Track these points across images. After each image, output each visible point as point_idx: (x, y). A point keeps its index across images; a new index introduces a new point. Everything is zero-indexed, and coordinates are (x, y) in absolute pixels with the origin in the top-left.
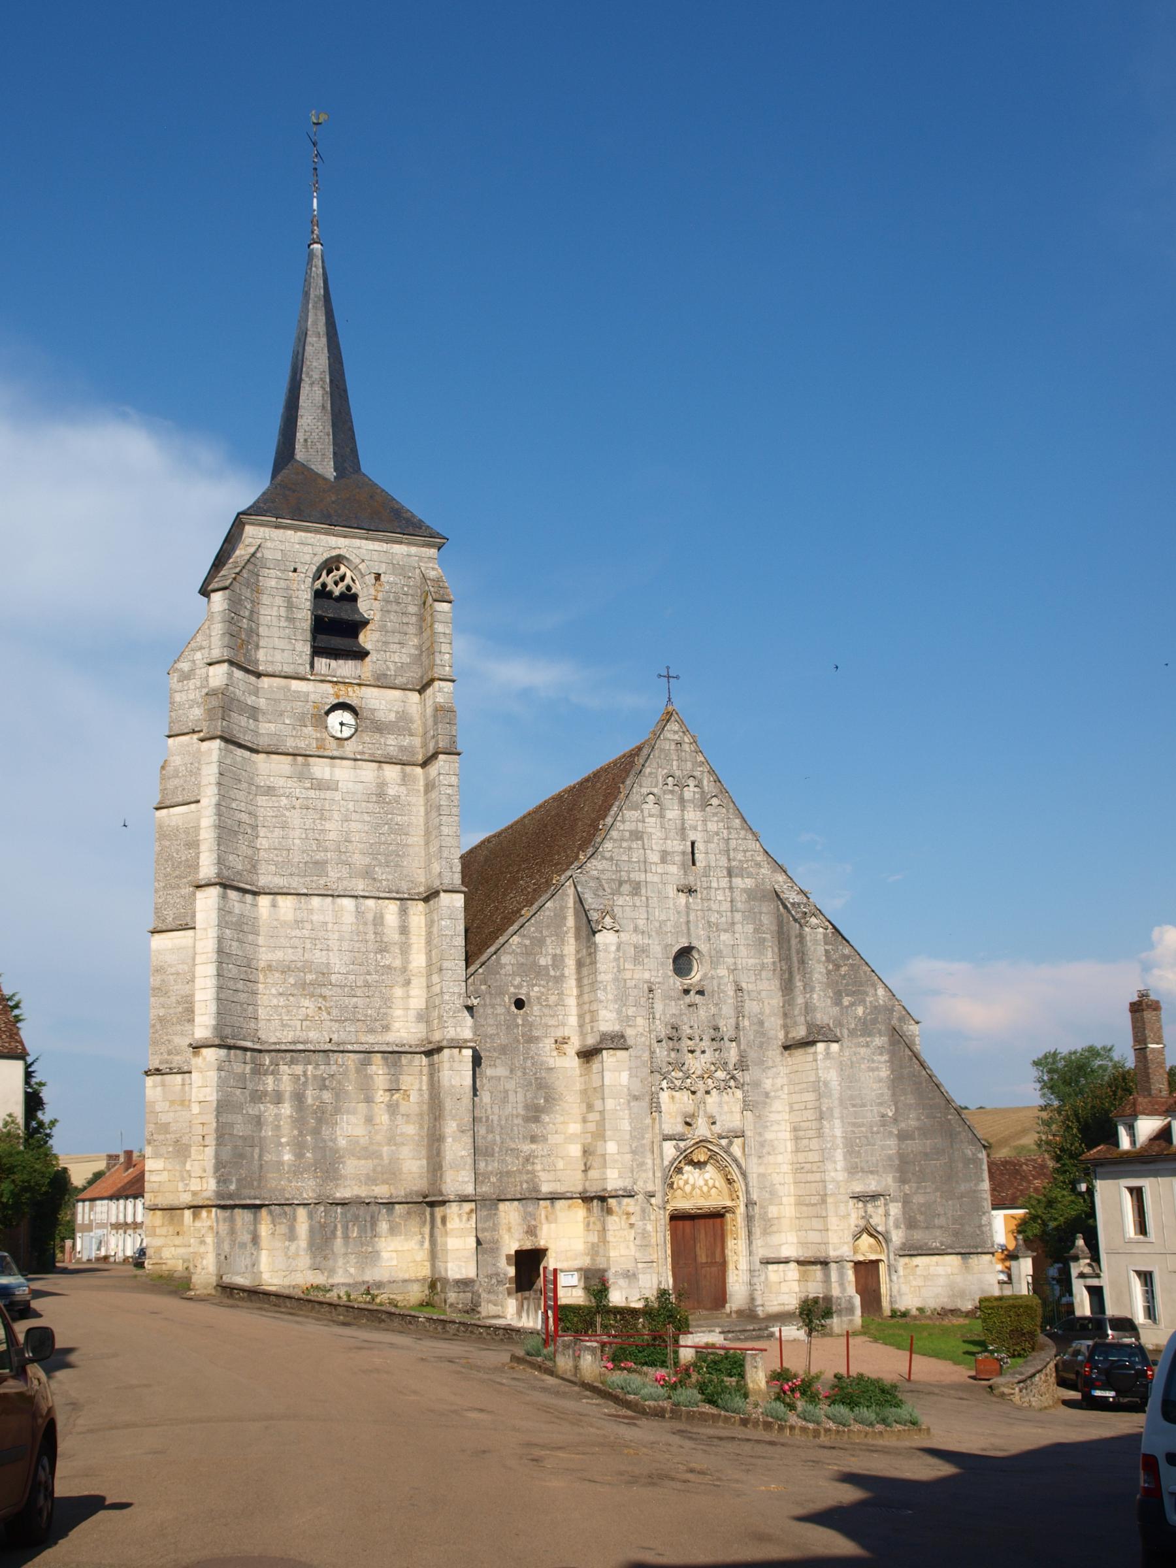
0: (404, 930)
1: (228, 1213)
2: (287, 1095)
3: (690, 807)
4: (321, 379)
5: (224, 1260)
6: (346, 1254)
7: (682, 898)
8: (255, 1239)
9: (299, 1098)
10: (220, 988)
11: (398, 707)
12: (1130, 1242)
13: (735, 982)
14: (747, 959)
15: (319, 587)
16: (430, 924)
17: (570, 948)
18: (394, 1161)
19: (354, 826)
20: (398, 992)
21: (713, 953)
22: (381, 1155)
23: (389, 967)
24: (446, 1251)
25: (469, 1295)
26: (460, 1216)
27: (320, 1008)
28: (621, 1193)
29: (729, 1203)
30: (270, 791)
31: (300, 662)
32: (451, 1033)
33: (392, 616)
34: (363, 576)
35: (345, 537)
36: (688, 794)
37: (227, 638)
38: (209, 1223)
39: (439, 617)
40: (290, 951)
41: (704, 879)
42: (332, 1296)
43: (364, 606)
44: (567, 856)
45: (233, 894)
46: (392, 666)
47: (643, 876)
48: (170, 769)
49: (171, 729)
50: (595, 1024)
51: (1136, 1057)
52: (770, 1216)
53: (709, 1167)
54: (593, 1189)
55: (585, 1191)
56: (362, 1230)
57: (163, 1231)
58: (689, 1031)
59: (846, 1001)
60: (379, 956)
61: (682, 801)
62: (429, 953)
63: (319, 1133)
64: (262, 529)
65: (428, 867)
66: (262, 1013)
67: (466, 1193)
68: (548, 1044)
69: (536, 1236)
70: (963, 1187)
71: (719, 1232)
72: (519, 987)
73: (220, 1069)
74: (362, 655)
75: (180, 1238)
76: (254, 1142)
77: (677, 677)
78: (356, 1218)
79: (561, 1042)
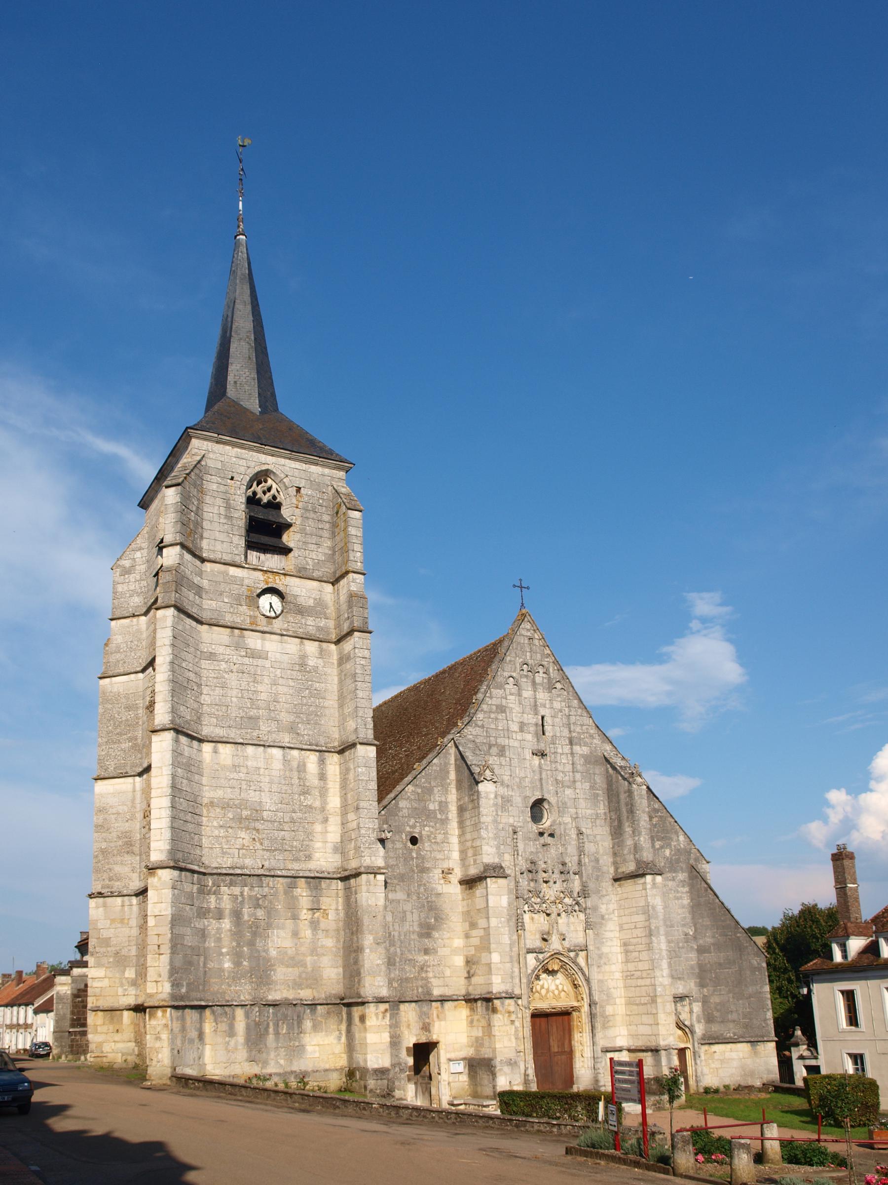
0: (322, 777)
1: (180, 1013)
2: (227, 912)
3: (540, 689)
4: (248, 337)
5: (177, 1054)
6: (277, 1048)
7: (536, 760)
8: (201, 1036)
9: (237, 915)
10: (173, 818)
12: (843, 1032)
13: (577, 828)
14: (585, 809)
15: (251, 494)
16: (345, 773)
17: (452, 796)
18: (316, 969)
19: (281, 689)
20: (318, 827)
21: (560, 804)
22: (306, 964)
23: (311, 807)
24: (364, 1044)
25: (385, 1082)
26: (377, 1014)
27: (254, 839)
28: (504, 995)
29: (576, 1004)
30: (212, 656)
31: (236, 552)
32: (367, 861)
33: (310, 522)
34: (287, 488)
35: (272, 456)
36: (540, 678)
37: (179, 525)
38: (164, 1022)
39: (352, 522)
40: (229, 790)
41: (552, 746)
42: (269, 1084)
43: (286, 513)
44: (437, 728)
45: (183, 739)
46: (310, 562)
47: (507, 741)
48: (112, 646)
49: (113, 613)
50: (478, 857)
51: (837, 894)
52: (607, 1013)
53: (559, 975)
54: (476, 992)
55: (468, 994)
56: (290, 1028)
57: (104, 1029)
58: (544, 866)
60: (302, 798)
61: (534, 683)
62: (344, 797)
63: (254, 945)
64: (206, 443)
65: (342, 725)
67: (381, 995)
68: (436, 874)
69: (430, 1032)
70: (751, 990)
71: (567, 1028)
72: (414, 827)
73: (174, 888)
75: (119, 1035)
76: (200, 951)
77: (528, 588)
78: (285, 1017)
79: (447, 873)
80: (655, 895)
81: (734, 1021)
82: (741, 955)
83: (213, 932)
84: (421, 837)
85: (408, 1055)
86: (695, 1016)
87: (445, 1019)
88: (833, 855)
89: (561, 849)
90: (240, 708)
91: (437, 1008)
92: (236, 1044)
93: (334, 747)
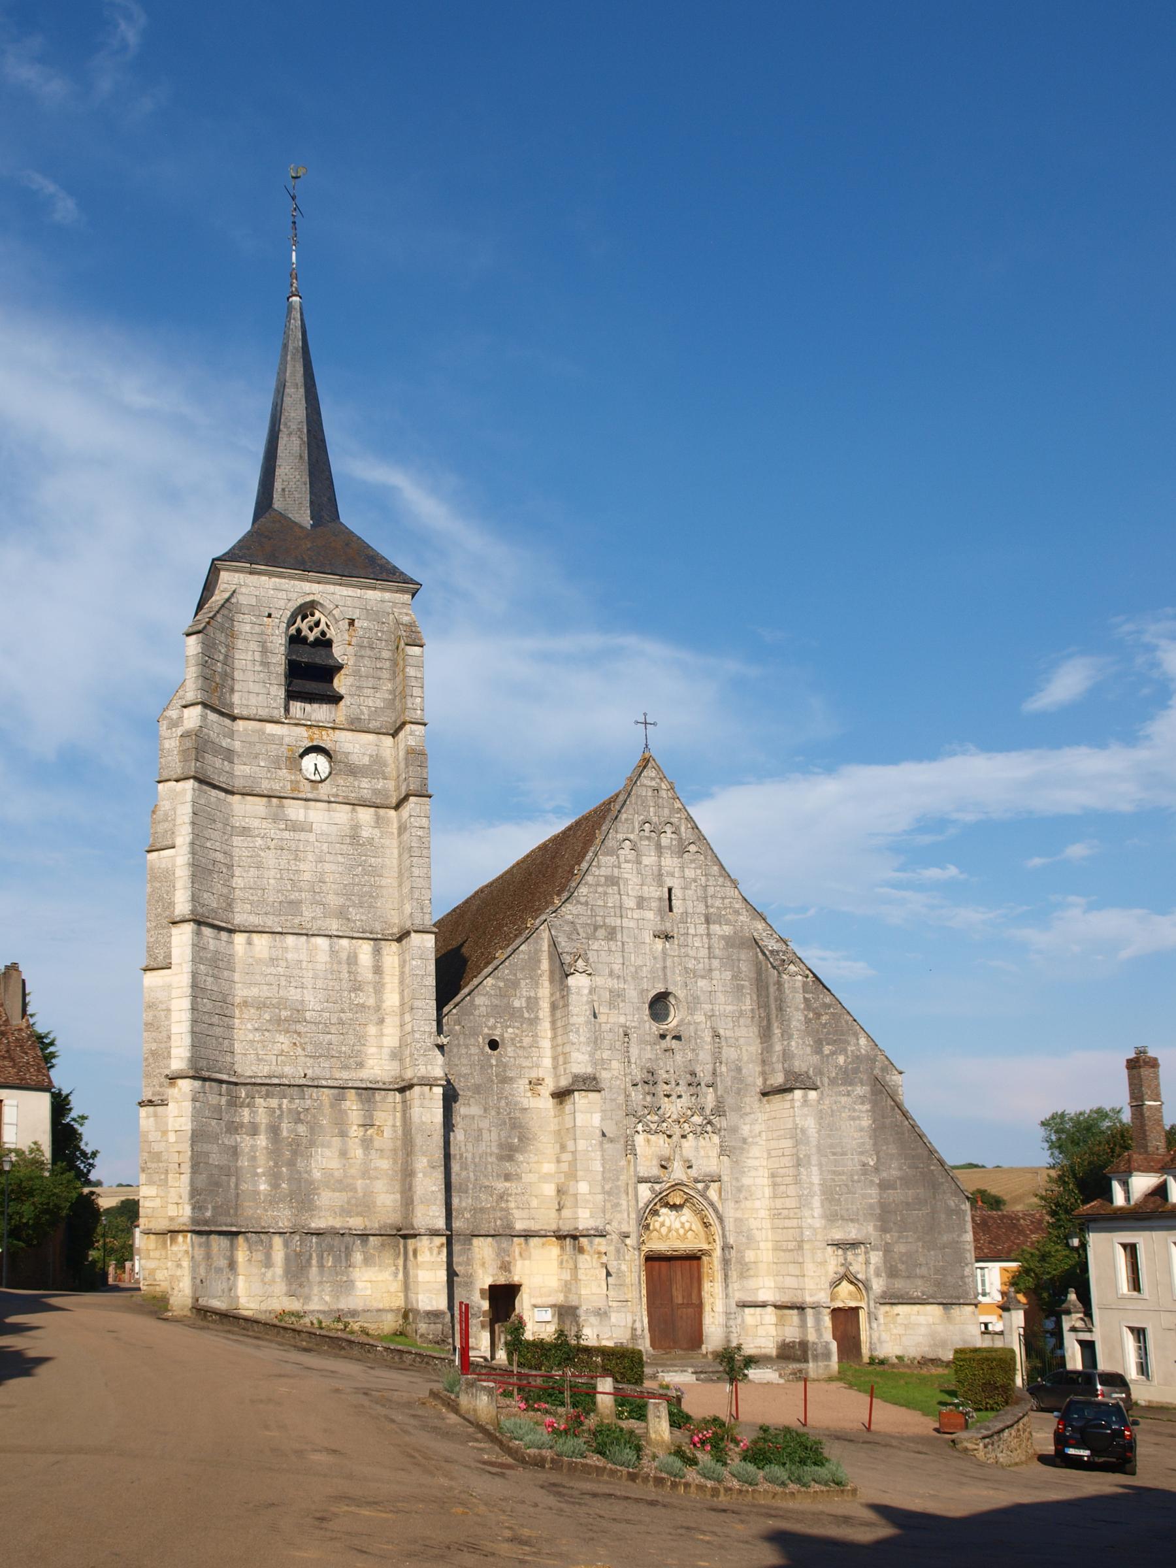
0: (378, 970)
1: (203, 1239)
2: (263, 1127)
4: (299, 430)
5: (199, 1284)
6: (321, 1283)
7: (659, 944)
8: (232, 1265)
9: (274, 1130)
10: (194, 1021)
11: (372, 750)
12: (1123, 1298)
13: (713, 1028)
14: (724, 1005)
17: (545, 991)
18: (368, 1194)
19: (328, 867)
20: (372, 1030)
23: (363, 1006)
24: (417, 1282)
25: (440, 1326)
26: (431, 1249)
28: (592, 1232)
29: (705, 1247)
30: (245, 831)
32: (422, 1071)
33: (366, 661)
36: (665, 840)
38: (185, 1248)
39: (410, 661)
40: (265, 987)
43: (337, 651)
45: (207, 931)
46: (366, 711)
48: (160, 813)
52: (747, 1260)
53: (685, 1210)
54: (566, 1228)
56: (337, 1260)
59: (827, 1050)
60: (353, 995)
61: (659, 847)
63: (295, 1165)
64: (237, 575)
66: (238, 1047)
68: (522, 1085)
69: (510, 1272)
70: (945, 1238)
73: (194, 1100)
74: (336, 699)
76: (230, 1171)
78: (331, 1249)
79: (535, 1083)
80: (806, 1115)
81: (923, 1277)
82: (934, 1193)
83: (247, 1150)
84: (503, 1040)
85: (482, 1298)
86: (872, 1268)
87: (530, 1258)
88: (1129, 1061)
89: (690, 1055)
90: (278, 891)
91: (520, 1244)
92: (273, 1276)
93: (392, 934)
